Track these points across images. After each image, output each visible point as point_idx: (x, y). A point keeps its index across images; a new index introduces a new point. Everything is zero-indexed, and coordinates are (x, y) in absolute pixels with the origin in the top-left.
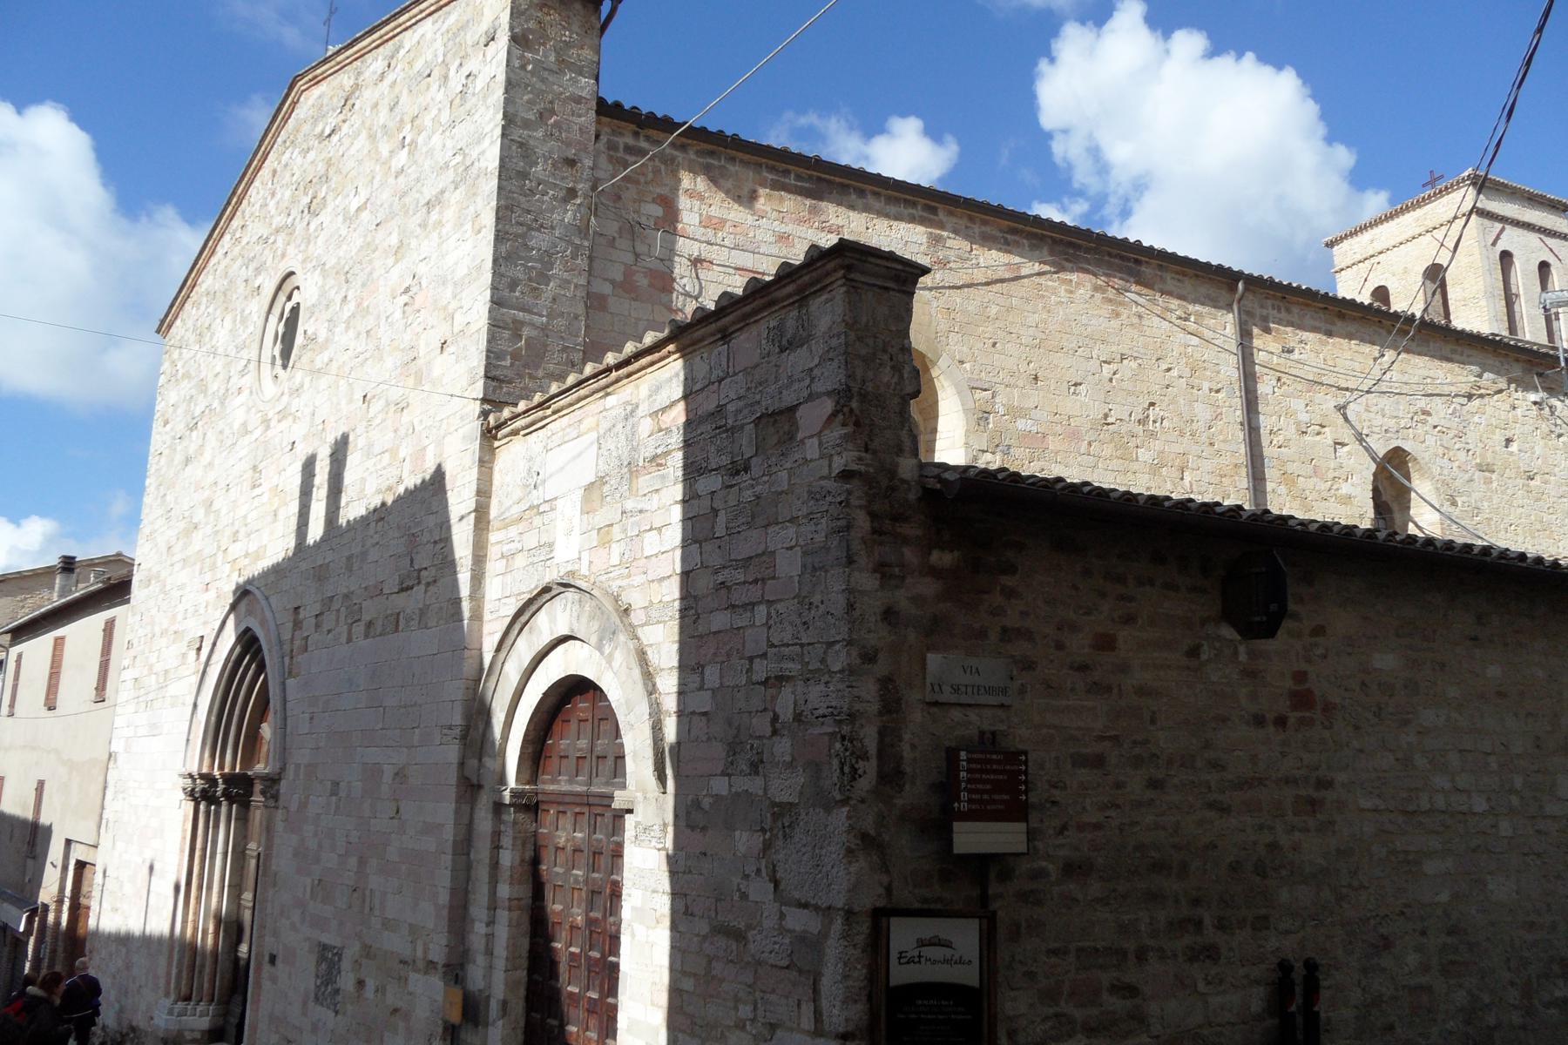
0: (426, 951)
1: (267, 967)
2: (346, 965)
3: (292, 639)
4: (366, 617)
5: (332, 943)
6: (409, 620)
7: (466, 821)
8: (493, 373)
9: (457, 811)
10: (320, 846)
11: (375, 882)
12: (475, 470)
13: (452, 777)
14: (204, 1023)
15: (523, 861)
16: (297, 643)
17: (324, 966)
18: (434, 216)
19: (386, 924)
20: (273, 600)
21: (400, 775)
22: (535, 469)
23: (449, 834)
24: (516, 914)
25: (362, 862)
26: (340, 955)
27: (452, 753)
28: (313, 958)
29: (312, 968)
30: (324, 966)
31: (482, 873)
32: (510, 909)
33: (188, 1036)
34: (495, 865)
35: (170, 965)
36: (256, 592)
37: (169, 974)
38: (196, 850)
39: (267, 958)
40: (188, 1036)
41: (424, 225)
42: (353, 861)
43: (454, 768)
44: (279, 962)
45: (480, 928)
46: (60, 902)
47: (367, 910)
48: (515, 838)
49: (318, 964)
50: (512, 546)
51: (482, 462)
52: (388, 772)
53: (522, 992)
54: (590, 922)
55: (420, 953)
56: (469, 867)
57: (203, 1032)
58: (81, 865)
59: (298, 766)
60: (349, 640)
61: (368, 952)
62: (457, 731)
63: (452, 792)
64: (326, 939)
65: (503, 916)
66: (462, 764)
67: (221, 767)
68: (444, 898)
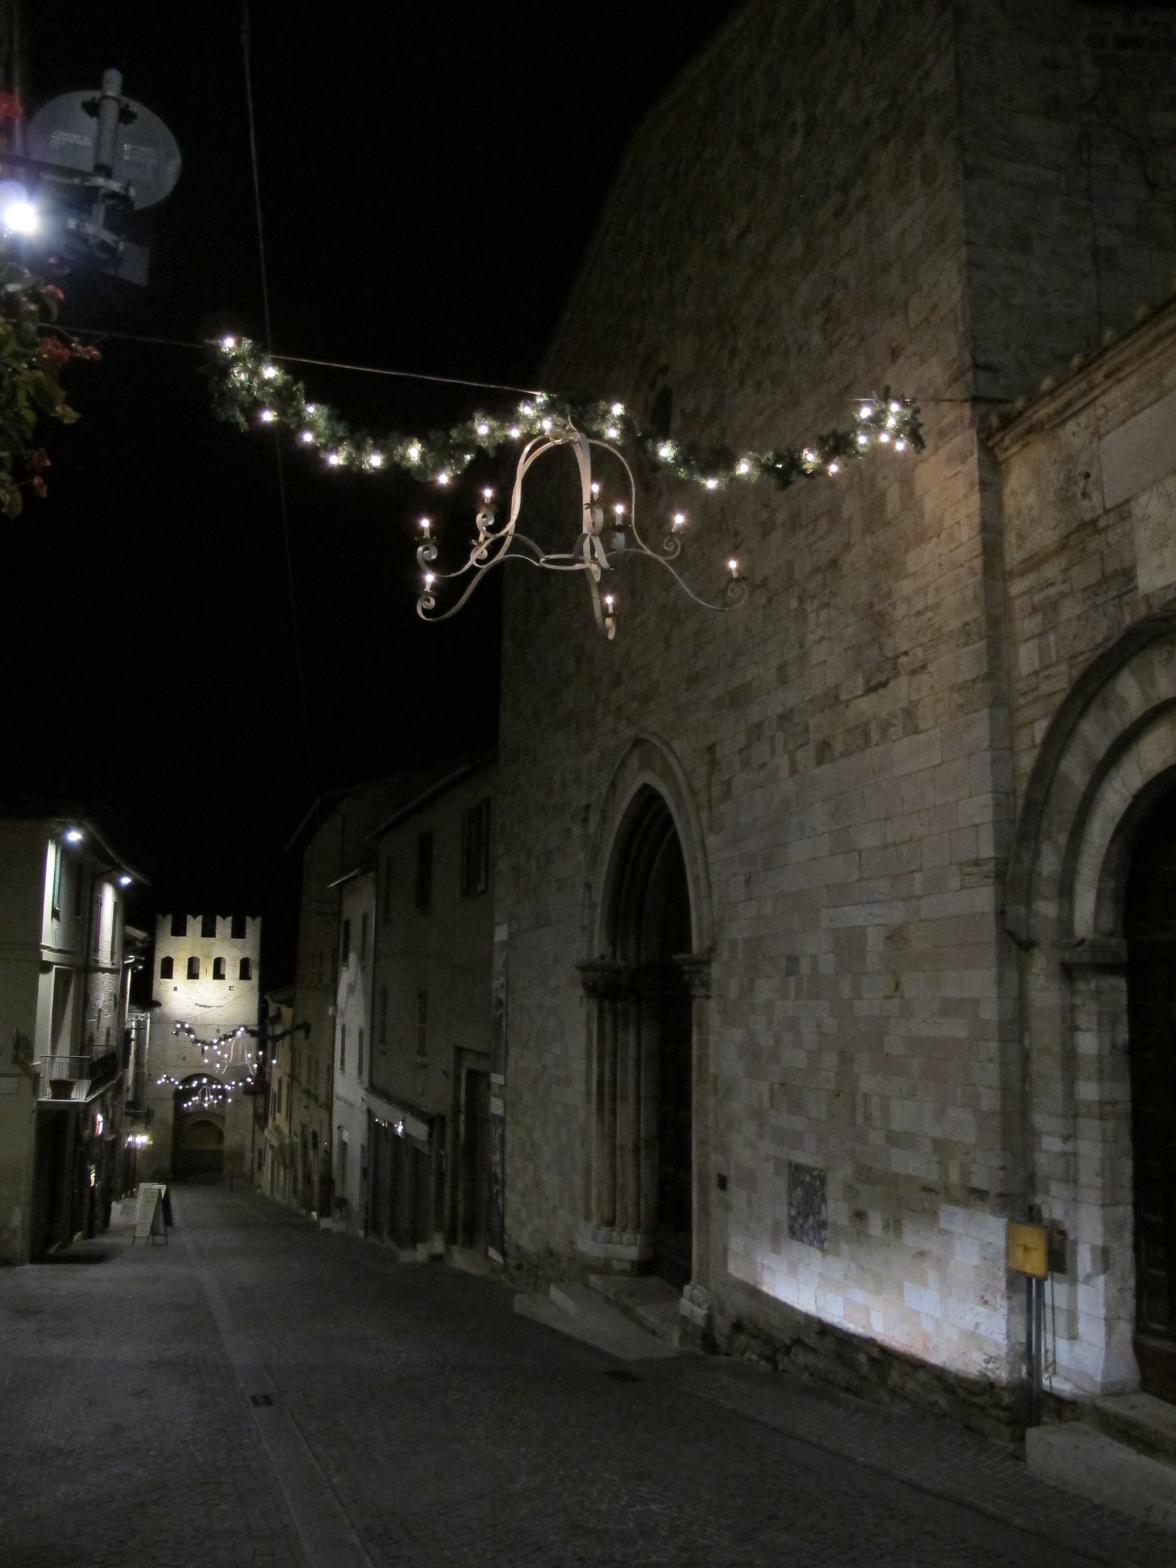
0: (965, 1173)
1: (715, 1193)
2: (833, 1189)
3: (709, 786)
4: (816, 737)
5: (811, 1164)
6: (885, 727)
7: (1013, 992)
8: (982, 359)
9: (1000, 981)
10: (778, 1042)
11: (868, 1083)
12: (975, 499)
13: (989, 931)
14: (632, 1253)
15: (1114, 1046)
16: (716, 791)
17: (799, 1192)
18: (857, 192)
19: (893, 1139)
20: (676, 745)
21: (895, 936)
22: (1081, 469)
23: (990, 1012)
24: (1111, 1124)
25: (846, 1059)
26: (823, 1180)
27: (984, 898)
28: (782, 1184)
29: (784, 1197)
30: (799, 1192)
31: (1046, 1066)
32: (1102, 1117)
33: (617, 1266)
34: (1070, 1057)
35: (587, 1185)
36: (654, 739)
37: (587, 1195)
38: (606, 1052)
39: (714, 1181)
40: (617, 1266)
41: (840, 211)
42: (830, 1060)
43: (990, 922)
44: (732, 1186)
45: (1052, 1144)
46: (456, 1111)
47: (860, 1120)
48: (1100, 1014)
49: (791, 1187)
50: (1052, 591)
51: (984, 485)
52: (874, 942)
53: (1128, 1238)
54: (806, 1217)
55: (954, 1176)
56: (1026, 1057)
57: (633, 1263)
58: (472, 1073)
59: (733, 944)
60: (794, 771)
61: (866, 1175)
62: (991, 866)
63: (991, 955)
64: (802, 1158)
65: (1090, 1128)
66: (1001, 913)
67: (624, 958)
68: (990, 1101)
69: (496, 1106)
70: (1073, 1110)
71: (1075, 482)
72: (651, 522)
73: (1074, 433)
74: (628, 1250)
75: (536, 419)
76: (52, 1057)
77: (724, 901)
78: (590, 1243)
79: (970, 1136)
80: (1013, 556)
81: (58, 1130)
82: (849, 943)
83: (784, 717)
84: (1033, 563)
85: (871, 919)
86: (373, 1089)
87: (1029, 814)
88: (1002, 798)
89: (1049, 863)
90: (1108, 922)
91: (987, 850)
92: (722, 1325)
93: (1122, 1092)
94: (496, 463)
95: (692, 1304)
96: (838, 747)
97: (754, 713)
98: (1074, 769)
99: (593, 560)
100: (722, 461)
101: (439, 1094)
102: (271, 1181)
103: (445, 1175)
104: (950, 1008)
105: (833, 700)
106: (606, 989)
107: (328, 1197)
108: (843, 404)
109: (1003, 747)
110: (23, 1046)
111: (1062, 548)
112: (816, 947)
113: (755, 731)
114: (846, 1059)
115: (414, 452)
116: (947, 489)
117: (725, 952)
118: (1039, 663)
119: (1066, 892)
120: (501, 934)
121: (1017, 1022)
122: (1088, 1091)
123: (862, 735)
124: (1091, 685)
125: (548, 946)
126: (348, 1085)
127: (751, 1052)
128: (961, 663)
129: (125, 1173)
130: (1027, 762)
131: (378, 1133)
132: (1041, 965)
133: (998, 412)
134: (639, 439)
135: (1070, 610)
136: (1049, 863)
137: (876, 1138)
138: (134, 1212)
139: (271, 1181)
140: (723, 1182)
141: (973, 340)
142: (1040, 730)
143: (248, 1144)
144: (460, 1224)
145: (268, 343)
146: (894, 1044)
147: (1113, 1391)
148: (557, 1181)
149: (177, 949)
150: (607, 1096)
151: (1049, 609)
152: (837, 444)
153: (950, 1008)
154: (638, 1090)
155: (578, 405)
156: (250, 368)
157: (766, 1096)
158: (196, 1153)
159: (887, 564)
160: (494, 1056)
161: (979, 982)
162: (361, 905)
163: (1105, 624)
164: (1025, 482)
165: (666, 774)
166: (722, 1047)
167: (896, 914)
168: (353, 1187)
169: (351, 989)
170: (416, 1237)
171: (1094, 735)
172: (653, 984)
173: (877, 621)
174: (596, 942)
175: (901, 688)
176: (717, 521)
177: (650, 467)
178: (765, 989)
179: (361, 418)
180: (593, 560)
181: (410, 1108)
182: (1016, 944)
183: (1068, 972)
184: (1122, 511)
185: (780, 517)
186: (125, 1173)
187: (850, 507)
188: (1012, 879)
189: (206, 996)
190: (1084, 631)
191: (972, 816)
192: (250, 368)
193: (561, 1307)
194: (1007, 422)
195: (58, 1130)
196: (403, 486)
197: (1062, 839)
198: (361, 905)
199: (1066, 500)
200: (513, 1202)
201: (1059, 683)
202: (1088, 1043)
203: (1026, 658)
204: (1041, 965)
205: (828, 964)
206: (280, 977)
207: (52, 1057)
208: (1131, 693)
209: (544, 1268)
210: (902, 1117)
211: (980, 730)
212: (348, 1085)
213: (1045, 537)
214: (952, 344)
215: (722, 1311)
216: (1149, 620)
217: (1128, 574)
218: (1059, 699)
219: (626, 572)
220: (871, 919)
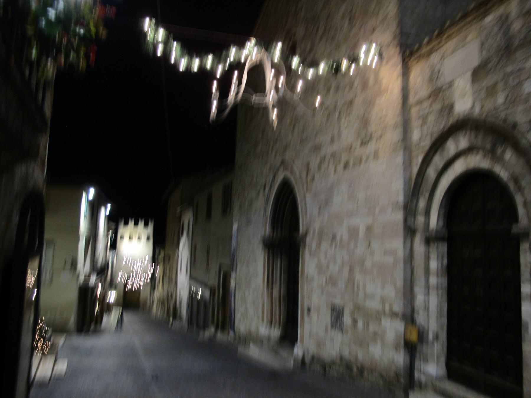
4: (343, 160)
25: (351, 271)
27: (399, 216)
31: (419, 272)
68: (400, 283)
69: (233, 284)
70: (427, 287)
71: (434, 76)
72: (291, 85)
73: (435, 58)
74: (276, 333)
75: (250, 52)
76: (83, 266)
77: (311, 216)
78: (263, 330)
79: (392, 294)
80: (412, 99)
81: (86, 293)
82: (353, 232)
83: (333, 155)
84: (419, 102)
85: (361, 223)
86: (191, 277)
87: (416, 188)
88: (407, 182)
89: (422, 204)
90: (441, 223)
91: (401, 199)
92: (308, 360)
93: (444, 281)
94: (238, 66)
95: (298, 351)
96: (351, 163)
97: (323, 152)
98: (431, 173)
99: (271, 97)
100: (315, 64)
101: (213, 280)
102: (156, 310)
103: (215, 310)
104: (386, 253)
105: (350, 149)
106: (271, 246)
107: (175, 314)
108: (356, 47)
109: (407, 164)
110: (74, 264)
111: (430, 97)
112: (342, 232)
113: (323, 160)
114: (351, 271)
115: (209, 60)
116: (390, 78)
117: (311, 232)
118: (421, 137)
119: (427, 213)
120: (235, 227)
121: (410, 257)
122: (433, 280)
123: (359, 161)
124: (438, 144)
125: (251, 233)
126: (183, 278)
127: (320, 269)
128: (393, 136)
129: (106, 308)
130: (415, 170)
131: (192, 297)
132: (418, 241)
133: (410, 48)
134: (286, 57)
135: (431, 118)
136: (422, 204)
137: (361, 294)
138: (110, 320)
139: (156, 310)
140: (309, 310)
141: (401, 24)
142: (420, 159)
143: (149, 298)
144: (220, 324)
145: (160, 21)
146: (368, 264)
147: (439, 379)
148: (253, 310)
149: (114, 8)
150: (270, 282)
151: (424, 119)
152: (354, 59)
153: (386, 253)
154: (280, 279)
155: (266, 44)
156: (154, 32)
157: (324, 282)
158: (130, 301)
159: (369, 104)
160: (232, 266)
161: (397, 244)
162: (188, 218)
163: (443, 123)
164: (419, 73)
165: (292, 172)
166: (309, 265)
167: (369, 220)
168: (184, 311)
169: (184, 245)
170: (205, 327)
171: (438, 161)
172: (286, 245)
173: (365, 122)
174: (267, 228)
175: (372, 146)
176: (311, 88)
177: (289, 70)
178: (325, 246)
179: (191, 49)
180: (271, 97)
181: (204, 284)
182: (410, 231)
183: (428, 241)
184: (450, 85)
185: (333, 85)
186: (106, 308)
187: (357, 83)
188: (409, 210)
189: (135, 247)
190: (435, 126)
191: (396, 189)
192: (154, 32)
193: (254, 352)
194: (411, 54)
195: (86, 293)
196: (205, 76)
197: (427, 195)
198: (188, 218)
199: (431, 80)
200: (238, 316)
201: (427, 143)
202: (434, 265)
203: (416, 135)
204: (418, 241)
205: (346, 237)
206: (162, 244)
207: (83, 266)
208: (452, 147)
209: (247, 339)
210: (370, 289)
211: (399, 159)
212: (183, 278)
213: (424, 92)
214: (393, 27)
215: (308, 351)
216: (457, 122)
217: (451, 107)
218: (427, 148)
219: (282, 103)
220: (361, 223)
